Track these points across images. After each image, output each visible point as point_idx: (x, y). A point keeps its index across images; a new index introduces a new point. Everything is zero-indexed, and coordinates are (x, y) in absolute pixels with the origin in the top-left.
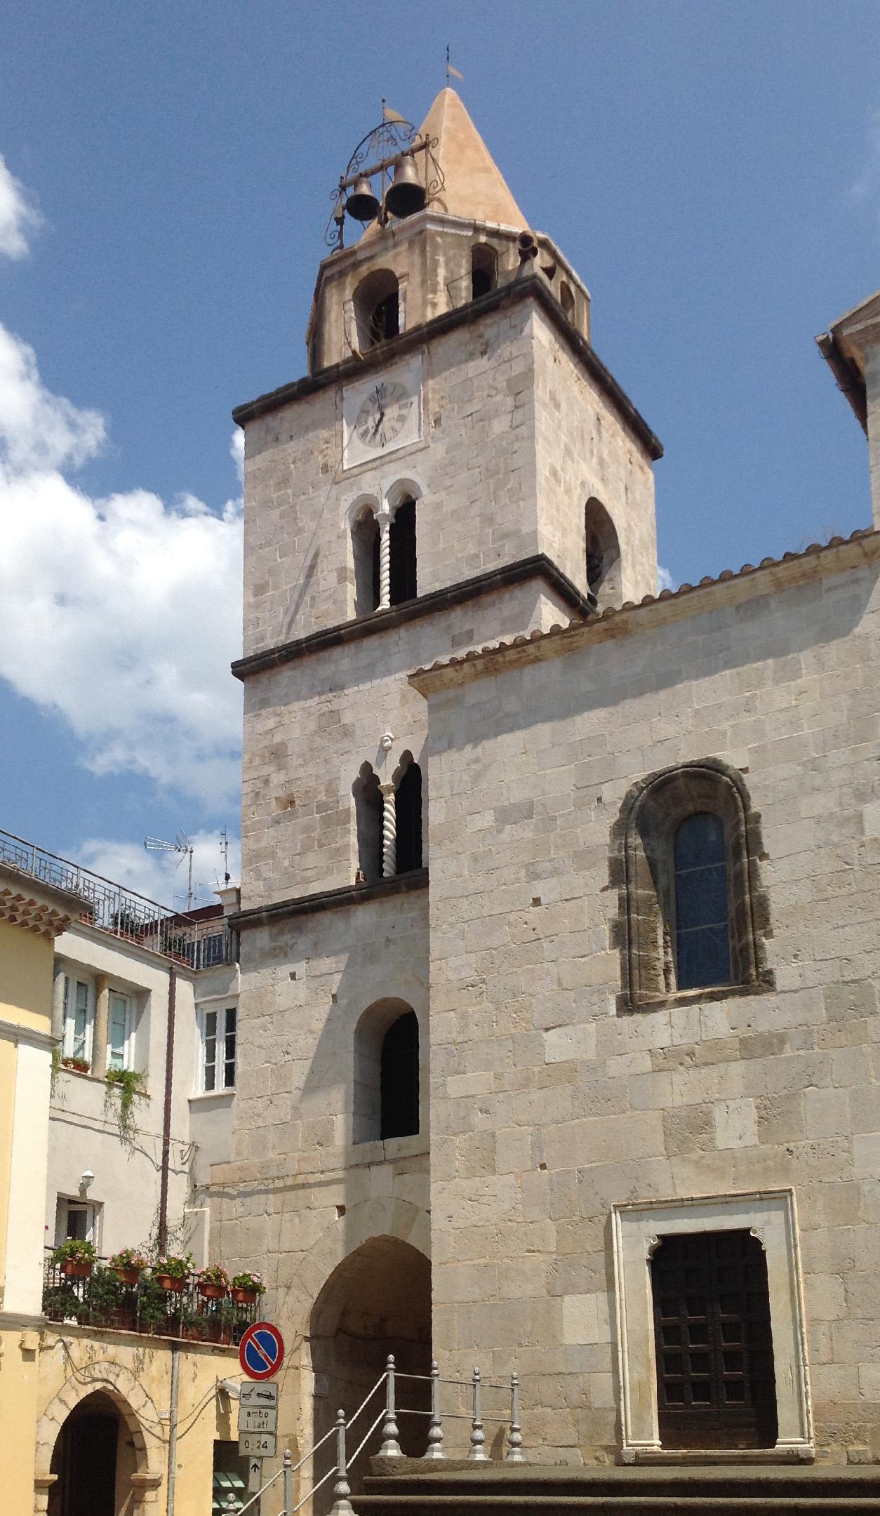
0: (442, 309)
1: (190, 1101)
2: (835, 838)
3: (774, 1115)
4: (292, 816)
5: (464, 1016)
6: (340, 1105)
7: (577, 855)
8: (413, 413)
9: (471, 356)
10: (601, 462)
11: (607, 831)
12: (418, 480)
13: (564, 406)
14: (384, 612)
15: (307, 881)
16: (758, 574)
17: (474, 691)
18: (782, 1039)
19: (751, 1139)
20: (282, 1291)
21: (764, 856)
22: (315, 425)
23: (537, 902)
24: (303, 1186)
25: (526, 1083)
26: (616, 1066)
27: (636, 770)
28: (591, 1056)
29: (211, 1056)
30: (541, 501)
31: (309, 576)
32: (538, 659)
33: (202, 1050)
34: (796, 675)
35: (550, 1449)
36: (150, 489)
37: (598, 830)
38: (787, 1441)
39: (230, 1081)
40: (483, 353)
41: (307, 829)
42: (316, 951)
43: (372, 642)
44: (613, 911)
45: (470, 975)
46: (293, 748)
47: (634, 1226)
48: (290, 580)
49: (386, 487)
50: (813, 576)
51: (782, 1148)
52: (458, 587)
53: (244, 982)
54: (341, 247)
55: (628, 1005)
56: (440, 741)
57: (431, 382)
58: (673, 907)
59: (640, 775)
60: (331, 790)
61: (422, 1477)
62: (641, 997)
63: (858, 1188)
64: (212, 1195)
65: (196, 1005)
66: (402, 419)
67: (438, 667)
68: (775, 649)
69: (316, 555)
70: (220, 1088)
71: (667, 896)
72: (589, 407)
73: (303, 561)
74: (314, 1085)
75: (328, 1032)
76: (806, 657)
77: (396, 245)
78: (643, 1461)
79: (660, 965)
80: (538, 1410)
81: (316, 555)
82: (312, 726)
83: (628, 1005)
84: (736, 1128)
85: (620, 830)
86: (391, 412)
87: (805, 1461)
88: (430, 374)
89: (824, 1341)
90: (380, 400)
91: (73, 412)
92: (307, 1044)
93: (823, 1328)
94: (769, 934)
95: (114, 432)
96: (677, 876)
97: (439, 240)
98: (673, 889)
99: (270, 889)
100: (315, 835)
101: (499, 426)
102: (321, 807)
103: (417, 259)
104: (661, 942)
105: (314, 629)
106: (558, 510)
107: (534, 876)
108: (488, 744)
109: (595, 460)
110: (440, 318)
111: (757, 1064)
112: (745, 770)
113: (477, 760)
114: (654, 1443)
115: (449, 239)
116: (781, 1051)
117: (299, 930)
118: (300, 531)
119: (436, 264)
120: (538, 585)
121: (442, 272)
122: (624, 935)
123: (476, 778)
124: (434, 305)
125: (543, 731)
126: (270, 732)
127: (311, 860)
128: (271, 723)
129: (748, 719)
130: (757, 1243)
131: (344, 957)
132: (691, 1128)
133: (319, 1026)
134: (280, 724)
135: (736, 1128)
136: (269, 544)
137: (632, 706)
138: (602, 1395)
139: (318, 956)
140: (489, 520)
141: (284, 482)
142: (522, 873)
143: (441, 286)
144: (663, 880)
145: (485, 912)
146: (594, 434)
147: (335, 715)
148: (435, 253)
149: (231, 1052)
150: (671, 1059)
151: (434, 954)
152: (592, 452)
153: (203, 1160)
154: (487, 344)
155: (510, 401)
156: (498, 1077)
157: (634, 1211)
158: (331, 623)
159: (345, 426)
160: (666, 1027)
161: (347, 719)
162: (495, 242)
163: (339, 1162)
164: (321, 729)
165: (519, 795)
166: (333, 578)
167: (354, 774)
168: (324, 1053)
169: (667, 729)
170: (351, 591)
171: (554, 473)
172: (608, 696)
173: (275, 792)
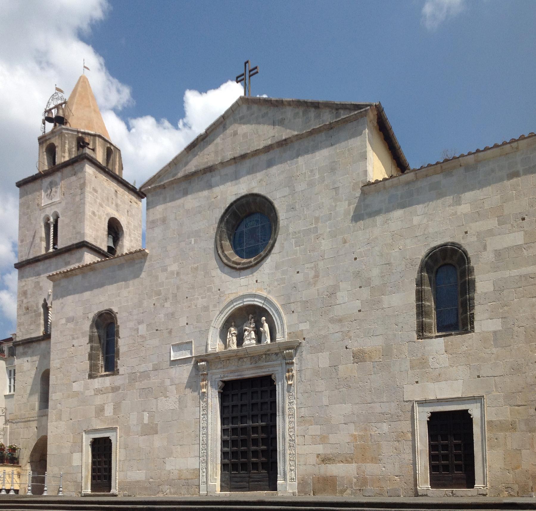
0: (67, 159)
1: (5, 396)
2: (133, 334)
3: (117, 408)
4: (28, 313)
5: (56, 377)
6: (37, 399)
7: (82, 333)
8: (59, 190)
9: (72, 175)
10: (117, 205)
11: (89, 327)
12: (59, 212)
13: (99, 191)
14: (51, 253)
15: (31, 333)
16: (121, 258)
17: (65, 283)
18: (119, 388)
19: (112, 414)
20: (24, 449)
21: (119, 337)
22: (35, 191)
23: (73, 346)
24: (29, 421)
25: (68, 397)
26: (87, 393)
27: (96, 310)
28: (82, 390)
29: (10, 383)
30: (87, 223)
31: (34, 238)
32: (76, 275)
33: (8, 380)
34: (128, 287)
35: (69, 493)
36: (153, 116)
37: (87, 325)
38: (113, 491)
39: (14, 391)
40: (75, 175)
41: (31, 317)
42: (32, 355)
43: (47, 261)
44: (89, 350)
45: (58, 366)
46: (29, 292)
47: (421, 408)
48: (29, 240)
49: (52, 213)
50: (133, 259)
51: (117, 416)
52: (66, 248)
53: (17, 361)
54: (44, 132)
55: (91, 377)
56: (56, 296)
57: (62, 182)
58: (105, 348)
59: (96, 312)
60: (37, 307)
61: (18, 499)
62: (94, 374)
63: (130, 427)
64: (9, 422)
65: (7, 368)
66: (56, 192)
67: (53, 275)
68: (125, 280)
69: (35, 232)
70: (12, 392)
71: (103, 347)
72: (112, 189)
73: (32, 233)
74: (31, 394)
75: (35, 379)
76: (131, 282)
77: (55, 136)
78: (86, 495)
79: (100, 365)
80: (67, 482)
81: (35, 232)
82: (33, 286)
83: (91, 377)
84: (109, 411)
85: (91, 327)
86: (54, 189)
87: (116, 496)
88: (62, 179)
89: (121, 466)
90: (52, 185)
91: (119, 85)
92: (30, 381)
93: (121, 463)
94: (119, 359)
95: (134, 95)
96: (107, 340)
97: (66, 135)
98: (105, 344)
99: (23, 335)
100: (33, 319)
101: (77, 199)
102: (35, 311)
103: (60, 141)
104: (101, 359)
105: (35, 256)
106: (95, 225)
107: (73, 339)
108: (65, 298)
109: (114, 205)
110: (65, 162)
111: (114, 394)
112: (117, 313)
113: (62, 303)
114: (89, 491)
115: (70, 135)
116: (119, 391)
117: (29, 347)
118: (31, 224)
119: (65, 143)
120: (84, 249)
121: (67, 146)
122: (91, 357)
123: (62, 308)
124: (64, 157)
125: (77, 296)
126: (23, 286)
127: (32, 327)
128: (24, 284)
129: (118, 298)
130: (110, 440)
131: (39, 356)
132: (100, 410)
133: (33, 376)
134: (26, 284)
135: (109, 411)
136: (24, 227)
137: (96, 291)
138: (79, 480)
139: (33, 356)
140: (74, 227)
141: (28, 207)
142: (71, 338)
143: (67, 151)
144: (102, 341)
145: (63, 347)
146: (114, 197)
147: (38, 283)
148: (65, 140)
149: (14, 380)
150: (98, 392)
151: (51, 359)
152: (112, 203)
153: (8, 413)
154: (75, 172)
155: (80, 191)
156: (63, 394)
157: (87, 432)
158: (39, 254)
159: (43, 193)
160: (97, 383)
161: (41, 284)
162: (84, 136)
163: (36, 415)
164: (35, 287)
165: (71, 314)
166: (39, 240)
167: (42, 302)
168: (34, 385)
169: (102, 299)
170: (44, 244)
171: (94, 213)
172: (90, 288)
173: (24, 305)
